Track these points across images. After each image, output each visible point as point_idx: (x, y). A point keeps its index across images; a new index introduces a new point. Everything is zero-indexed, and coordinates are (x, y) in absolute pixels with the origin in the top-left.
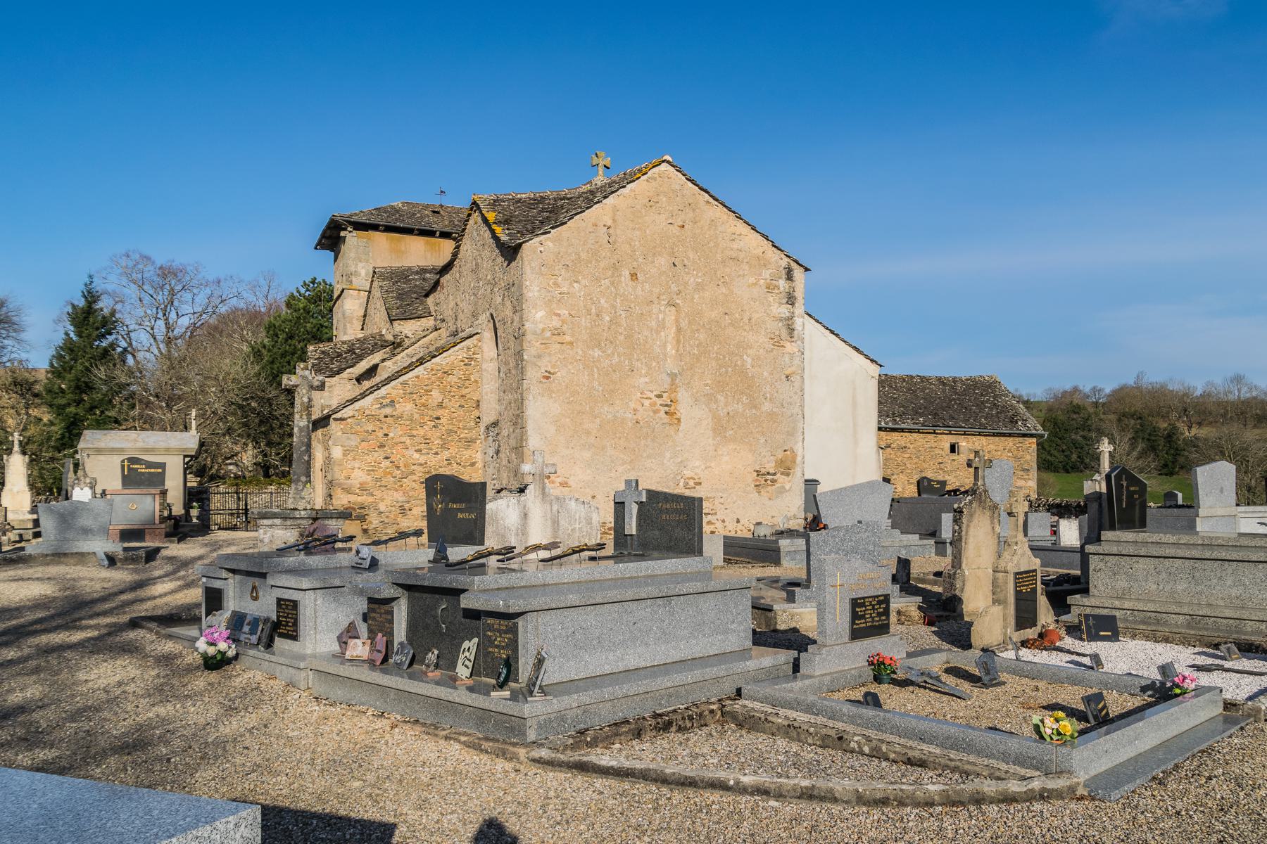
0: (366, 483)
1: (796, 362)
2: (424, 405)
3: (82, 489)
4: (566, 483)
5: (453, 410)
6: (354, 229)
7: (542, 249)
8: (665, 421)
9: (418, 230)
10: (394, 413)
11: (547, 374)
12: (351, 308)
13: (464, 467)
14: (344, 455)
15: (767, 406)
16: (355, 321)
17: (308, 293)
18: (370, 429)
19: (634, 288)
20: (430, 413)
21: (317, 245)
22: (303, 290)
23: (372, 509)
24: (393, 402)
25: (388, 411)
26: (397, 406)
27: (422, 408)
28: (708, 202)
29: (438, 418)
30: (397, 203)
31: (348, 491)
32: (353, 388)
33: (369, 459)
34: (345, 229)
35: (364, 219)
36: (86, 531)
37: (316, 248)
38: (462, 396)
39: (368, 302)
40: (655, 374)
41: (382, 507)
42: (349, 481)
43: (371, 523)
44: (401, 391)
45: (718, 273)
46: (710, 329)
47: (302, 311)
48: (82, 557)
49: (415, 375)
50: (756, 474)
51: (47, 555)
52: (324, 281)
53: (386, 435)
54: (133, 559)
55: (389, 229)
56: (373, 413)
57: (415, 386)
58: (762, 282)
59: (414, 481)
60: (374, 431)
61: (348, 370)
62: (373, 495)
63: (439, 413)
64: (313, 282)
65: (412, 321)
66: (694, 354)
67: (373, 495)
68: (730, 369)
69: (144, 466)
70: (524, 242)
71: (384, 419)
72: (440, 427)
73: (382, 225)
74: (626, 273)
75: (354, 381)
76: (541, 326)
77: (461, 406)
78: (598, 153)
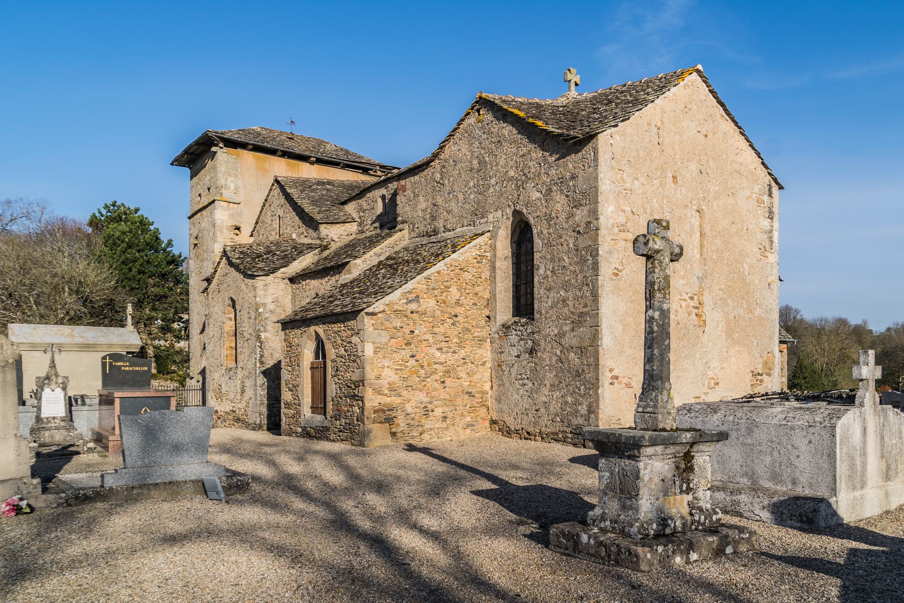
0: (394, 383)
1: (390, 290)
2: (444, 302)
3: (53, 391)
4: (630, 384)
5: (468, 308)
6: (225, 146)
7: (612, 142)
8: (696, 323)
9: (282, 151)
10: (419, 309)
11: (616, 271)
12: (222, 218)
13: (477, 366)
14: (375, 352)
15: (758, 311)
16: (225, 231)
17: (109, 214)
18: (399, 325)
19: (676, 190)
20: (449, 310)
21: (175, 160)
22: (104, 212)
23: (399, 412)
24: (417, 297)
25: (413, 306)
26: (421, 301)
27: (443, 305)
28: (722, 116)
29: (456, 316)
30: (256, 128)
31: (379, 392)
32: (286, 287)
33: (397, 357)
34: (217, 145)
35: (235, 137)
36: (177, 448)
37: (172, 164)
38: (476, 294)
39: (262, 209)
40: (689, 277)
41: (409, 408)
42: (380, 381)
43: (398, 425)
44: (425, 286)
45: (728, 183)
46: (723, 236)
47: (138, 224)
48: (173, 488)
49: (437, 270)
50: (751, 374)
51: (133, 488)
52: (123, 205)
53: (412, 332)
54: (238, 486)
55: (257, 149)
56: (401, 309)
57: (437, 281)
58: (754, 195)
59: (436, 380)
60: (402, 327)
61: (282, 270)
62: (400, 396)
63: (458, 310)
64: (114, 205)
65: (338, 225)
66: (714, 259)
67: (400, 396)
68: (736, 275)
69: (128, 364)
70: (598, 133)
71: (410, 315)
72: (458, 325)
73: (251, 144)
74: (670, 175)
75: (287, 281)
76: (612, 221)
77: (474, 304)
78: (571, 69)
